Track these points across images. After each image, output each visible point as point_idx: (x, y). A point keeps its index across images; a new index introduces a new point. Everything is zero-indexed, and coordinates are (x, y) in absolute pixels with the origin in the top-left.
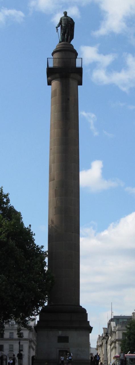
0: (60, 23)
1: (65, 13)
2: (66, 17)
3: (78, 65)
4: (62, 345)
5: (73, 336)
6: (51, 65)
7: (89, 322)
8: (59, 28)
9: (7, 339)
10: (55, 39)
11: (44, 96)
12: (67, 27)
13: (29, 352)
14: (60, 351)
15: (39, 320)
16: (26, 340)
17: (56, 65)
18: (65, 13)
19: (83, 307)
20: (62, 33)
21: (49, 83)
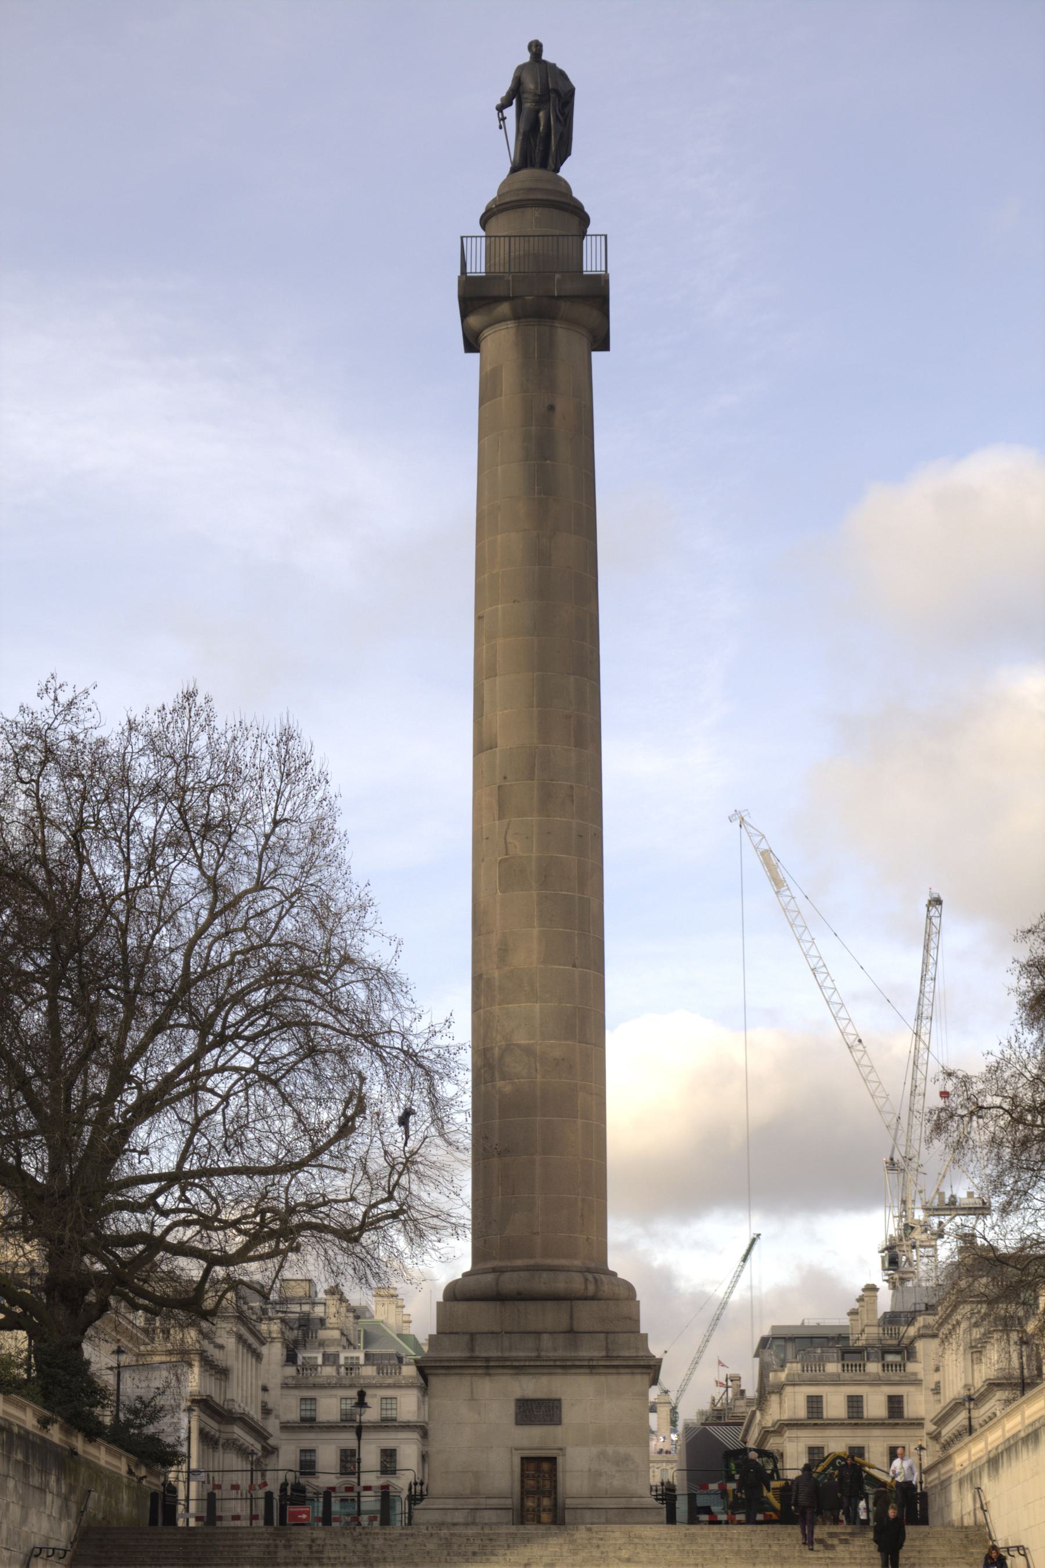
0: (516, 93)
1: (536, 48)
3: (591, 264)
4: (534, 1438)
5: (583, 1400)
6: (477, 267)
8: (511, 112)
9: (330, 1427)
10: (490, 158)
12: (543, 107)
16: (407, 1426)
18: (536, 48)
21: (471, 344)
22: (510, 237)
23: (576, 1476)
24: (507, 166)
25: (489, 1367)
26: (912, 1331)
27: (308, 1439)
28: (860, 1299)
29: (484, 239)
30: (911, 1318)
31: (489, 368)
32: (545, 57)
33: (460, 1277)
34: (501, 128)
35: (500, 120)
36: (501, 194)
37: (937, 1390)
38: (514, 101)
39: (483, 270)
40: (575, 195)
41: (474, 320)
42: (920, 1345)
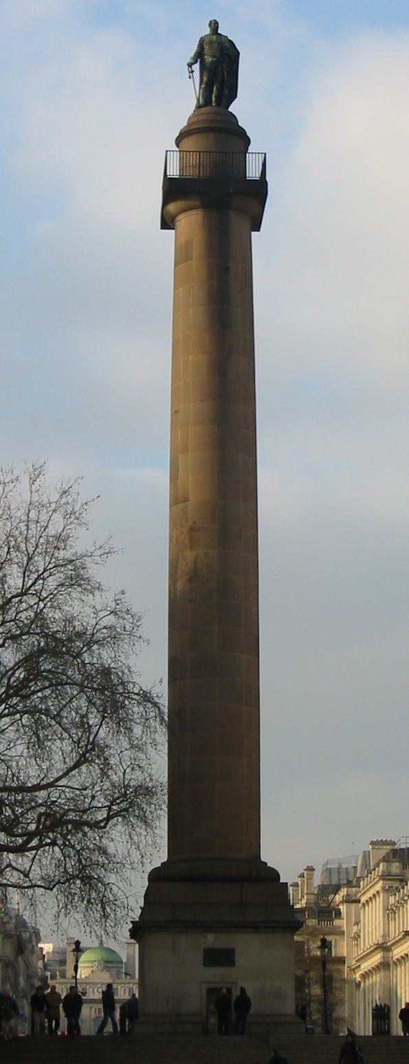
0: (199, 55)
1: (214, 26)
2: (215, 38)
4: (215, 975)
6: (174, 172)
8: (196, 67)
10: (183, 98)
12: (219, 66)
17: (191, 173)
18: (214, 26)
21: (167, 223)
22: (200, 152)
24: (193, 107)
25: (187, 927)
26: (338, 898)
28: (302, 876)
29: (178, 153)
30: (336, 889)
31: (183, 241)
32: (219, 32)
33: (159, 865)
34: (190, 77)
35: (190, 72)
36: (189, 124)
38: (199, 60)
39: (178, 174)
40: (240, 124)
41: (172, 207)
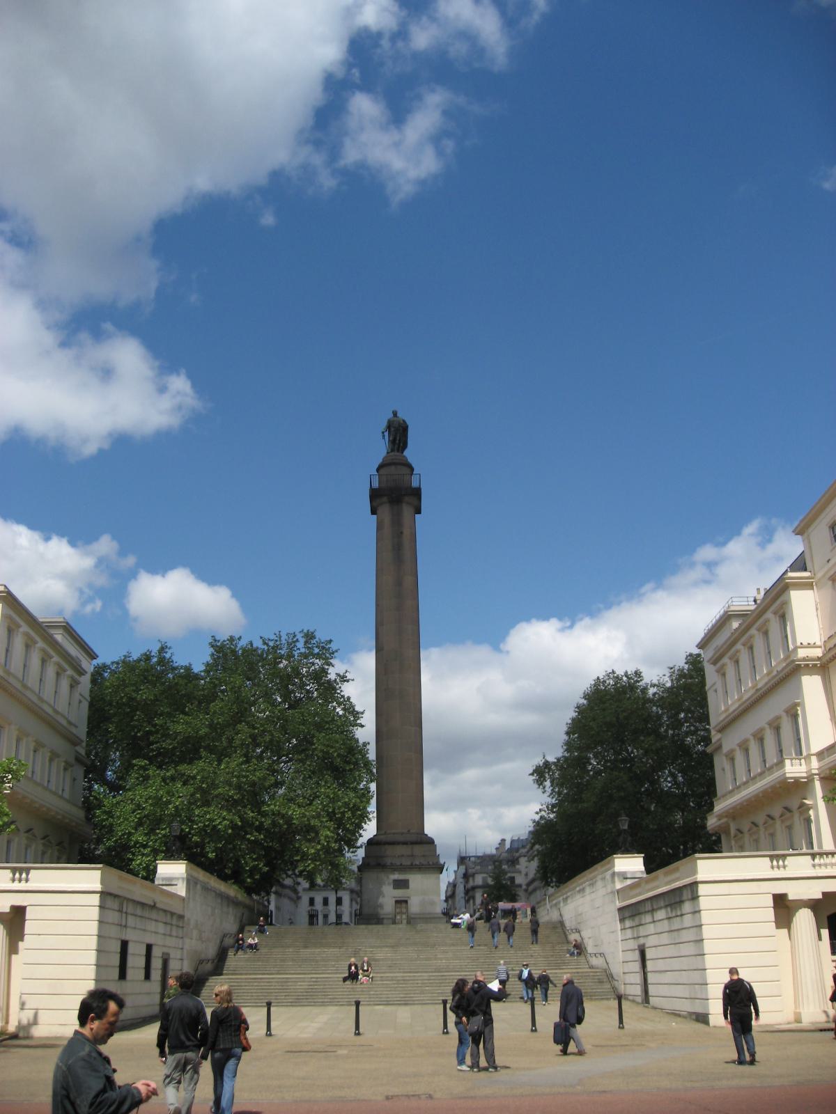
0: (389, 427)
1: (395, 414)
3: (415, 484)
4: (400, 893)
5: (417, 881)
6: (376, 485)
7: (824, 894)
8: (386, 434)
10: (379, 449)
11: (364, 527)
12: (398, 434)
13: (351, 906)
14: (397, 902)
15: (20, 943)
18: (395, 414)
19: (429, 836)
20: (391, 439)
23: (415, 906)
27: (312, 894)
28: (500, 844)
37: (526, 875)
41: (374, 504)
42: (351, 155)
